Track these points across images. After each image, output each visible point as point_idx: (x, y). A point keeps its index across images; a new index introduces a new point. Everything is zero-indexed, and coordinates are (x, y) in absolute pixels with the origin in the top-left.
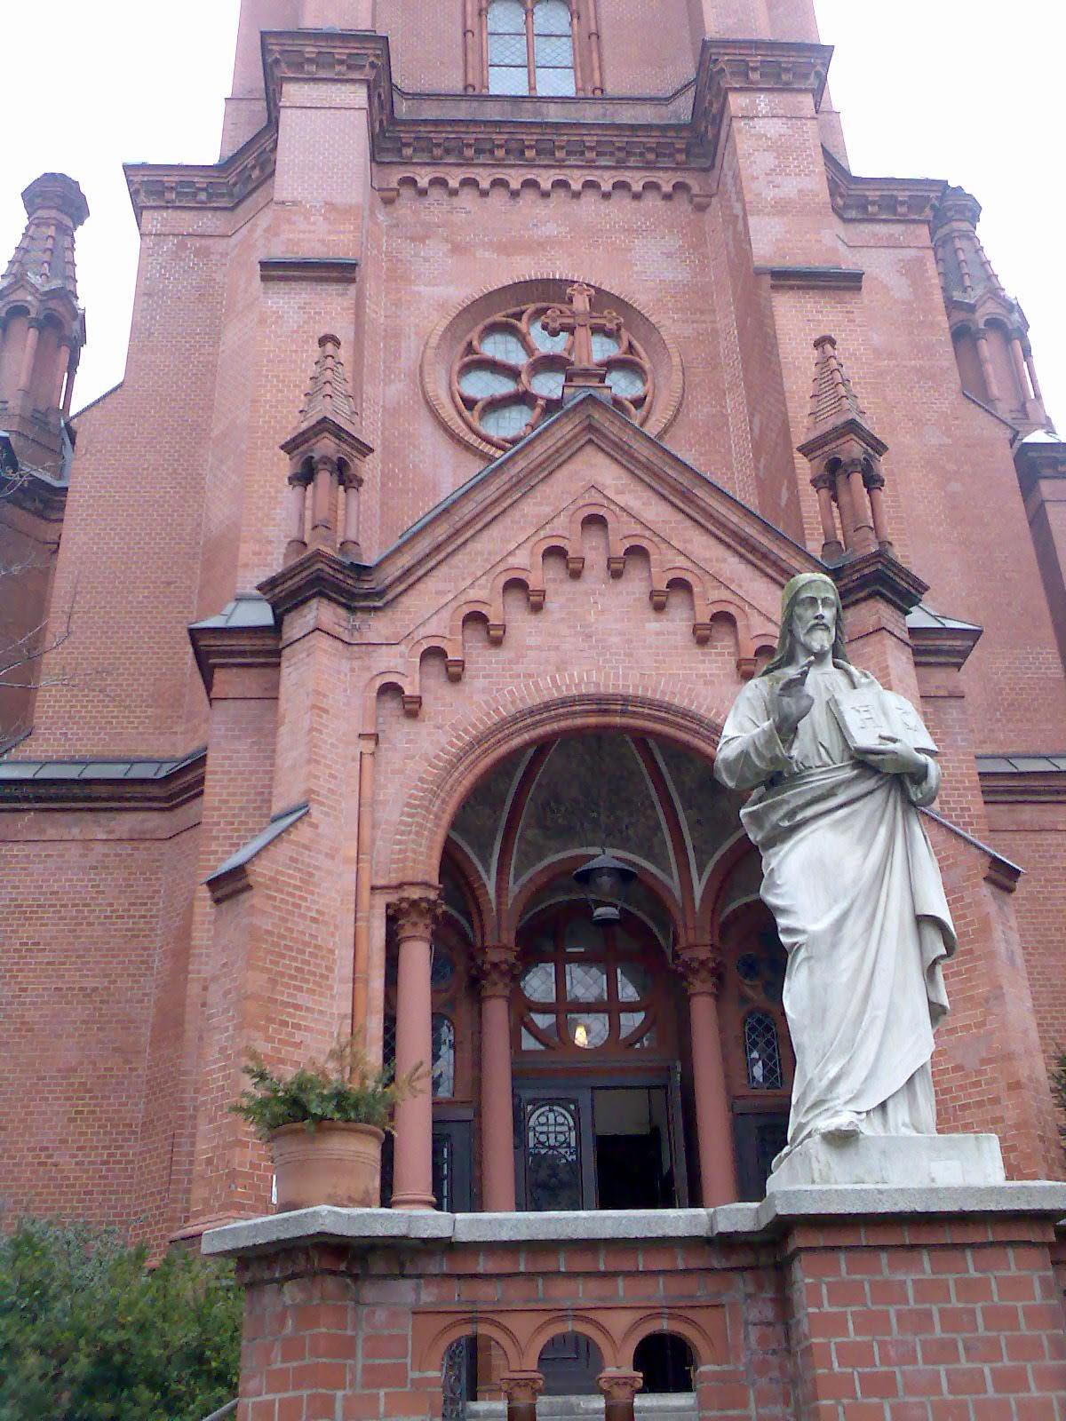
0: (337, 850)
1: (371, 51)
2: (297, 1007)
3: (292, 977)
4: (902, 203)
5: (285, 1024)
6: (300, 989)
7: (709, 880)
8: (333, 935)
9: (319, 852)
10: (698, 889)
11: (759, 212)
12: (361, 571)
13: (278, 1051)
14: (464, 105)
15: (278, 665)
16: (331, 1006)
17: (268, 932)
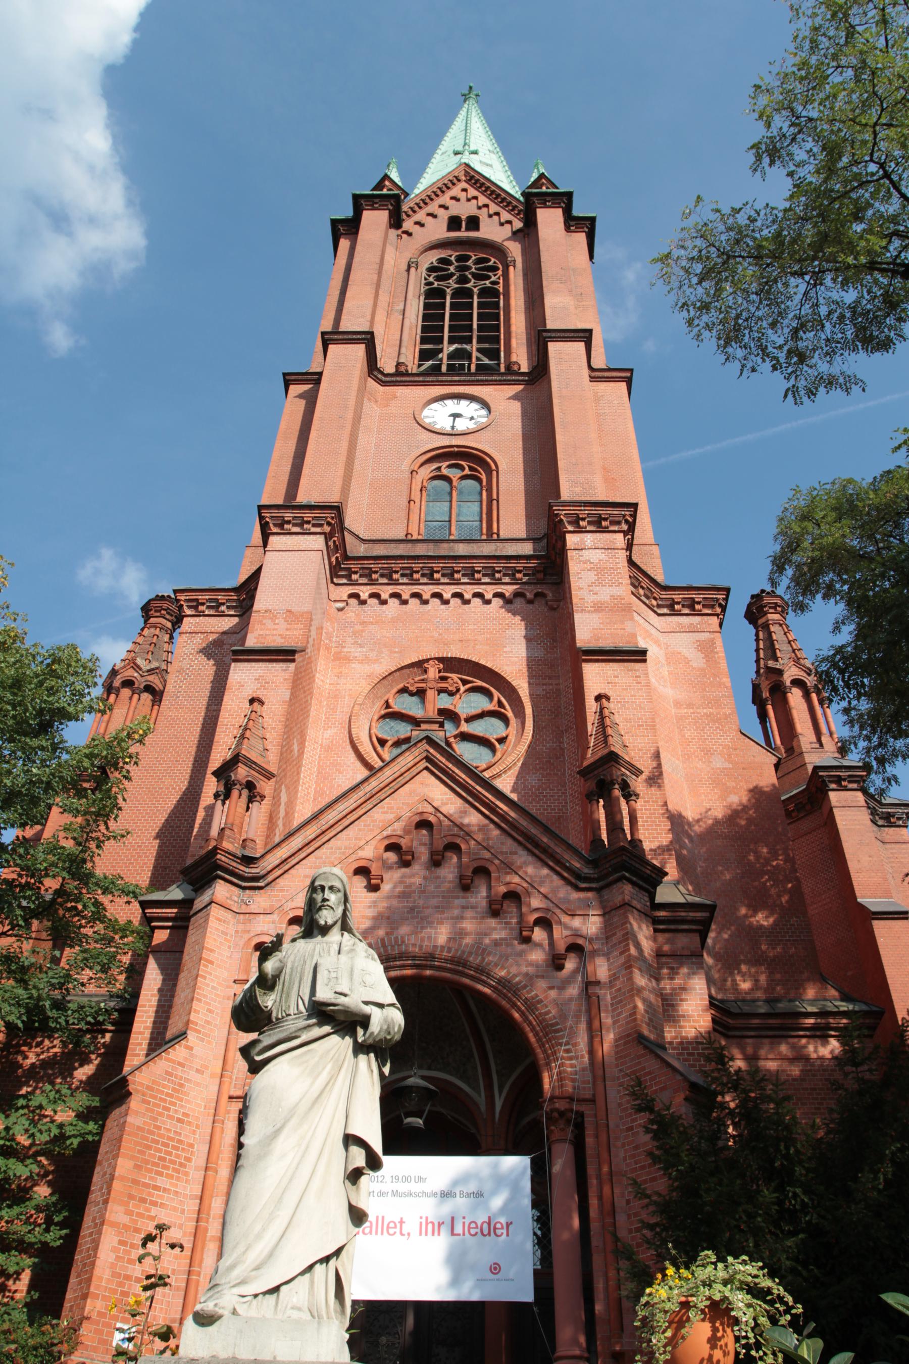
0: (206, 1067)
1: (329, 515)
2: (156, 1188)
3: (155, 1164)
4: (699, 603)
5: (143, 1200)
6: (161, 1174)
7: (508, 1094)
8: (194, 1132)
9: (191, 1068)
10: (498, 1108)
11: (582, 611)
12: (248, 861)
13: (136, 1222)
14: (402, 546)
15: (187, 928)
16: (185, 1188)
17: (139, 1128)
